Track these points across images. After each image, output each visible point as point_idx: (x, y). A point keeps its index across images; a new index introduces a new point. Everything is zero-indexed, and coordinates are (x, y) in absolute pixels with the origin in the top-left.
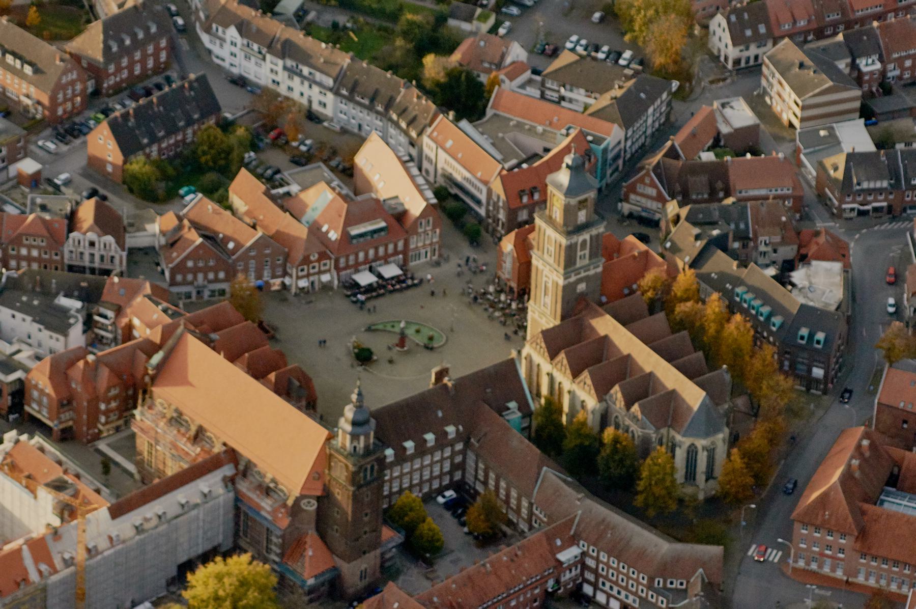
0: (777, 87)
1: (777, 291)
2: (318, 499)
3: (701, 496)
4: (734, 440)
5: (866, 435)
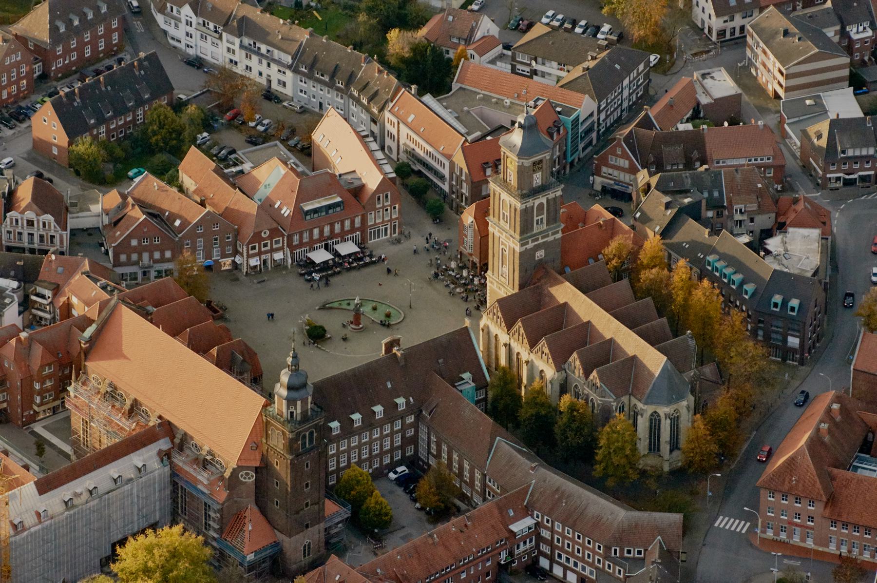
0: (762, 56)
1: (750, 258)
2: (257, 470)
3: (666, 468)
4: (699, 408)
5: (838, 399)
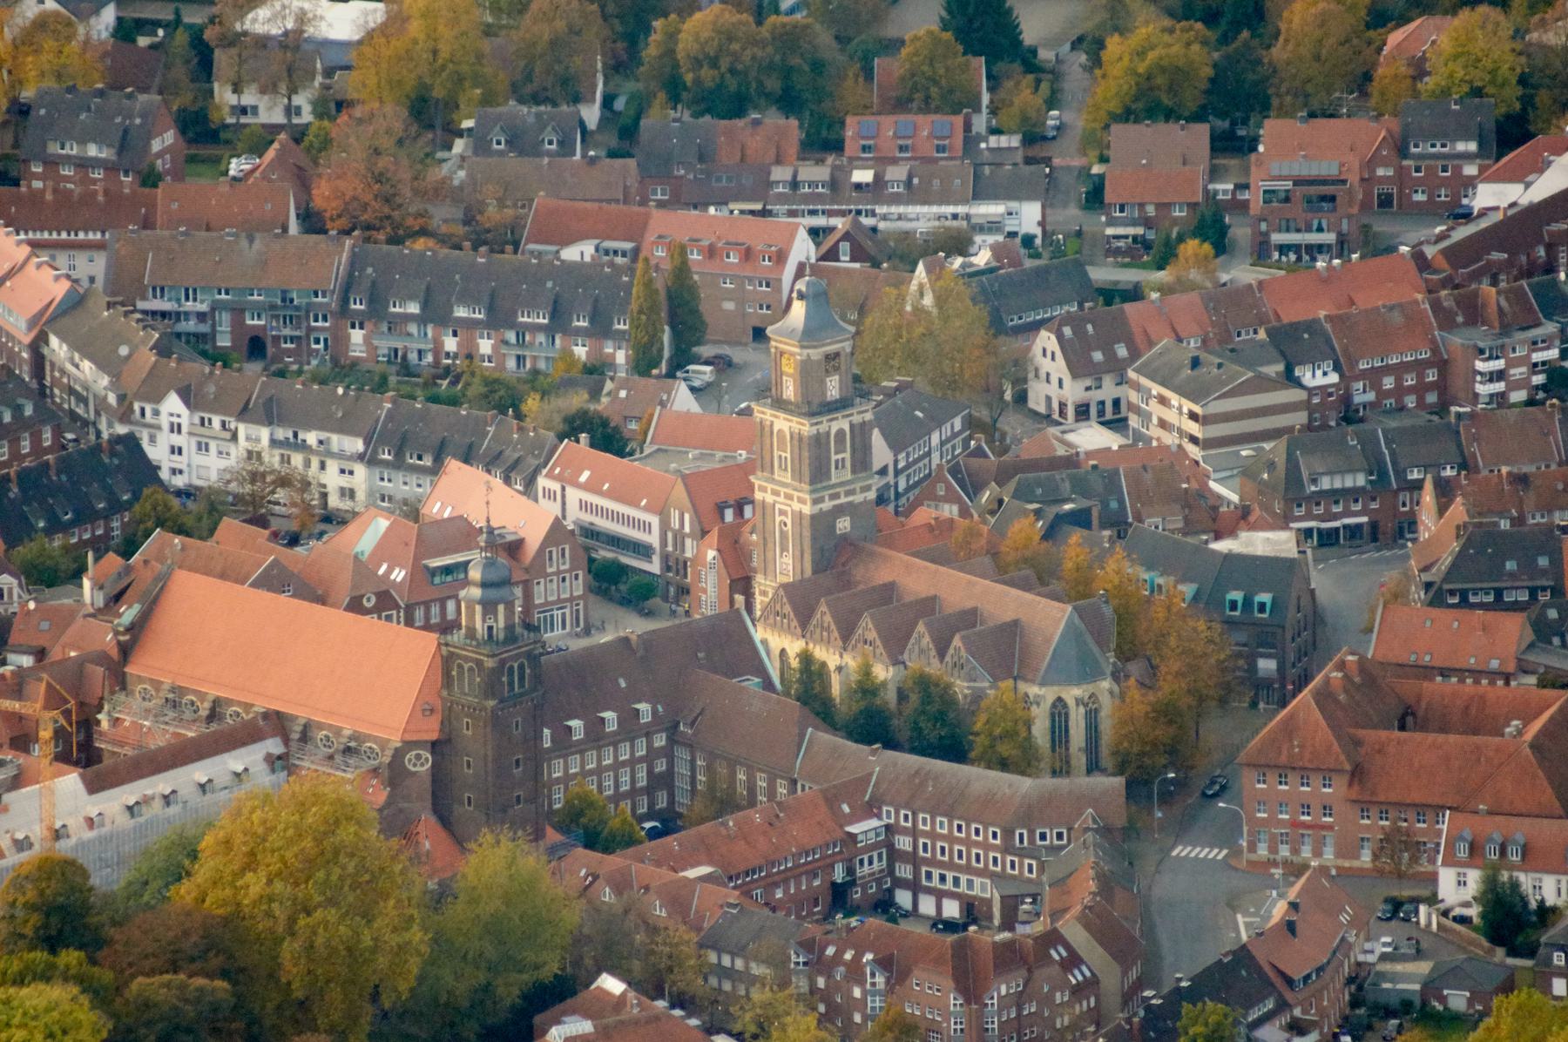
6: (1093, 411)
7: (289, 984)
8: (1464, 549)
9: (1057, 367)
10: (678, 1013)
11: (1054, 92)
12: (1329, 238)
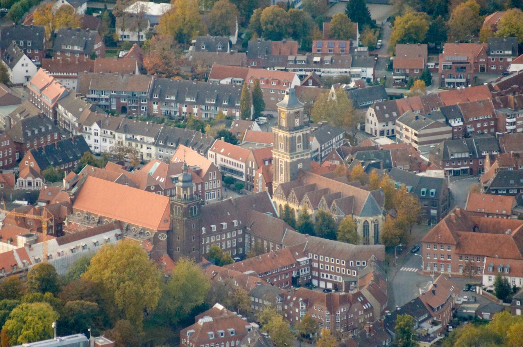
2: (168, 232)
6: (385, 133)
7: (117, 304)
8: (497, 176)
9: (374, 119)
10: (240, 316)
11: (380, 34)
12: (463, 80)
